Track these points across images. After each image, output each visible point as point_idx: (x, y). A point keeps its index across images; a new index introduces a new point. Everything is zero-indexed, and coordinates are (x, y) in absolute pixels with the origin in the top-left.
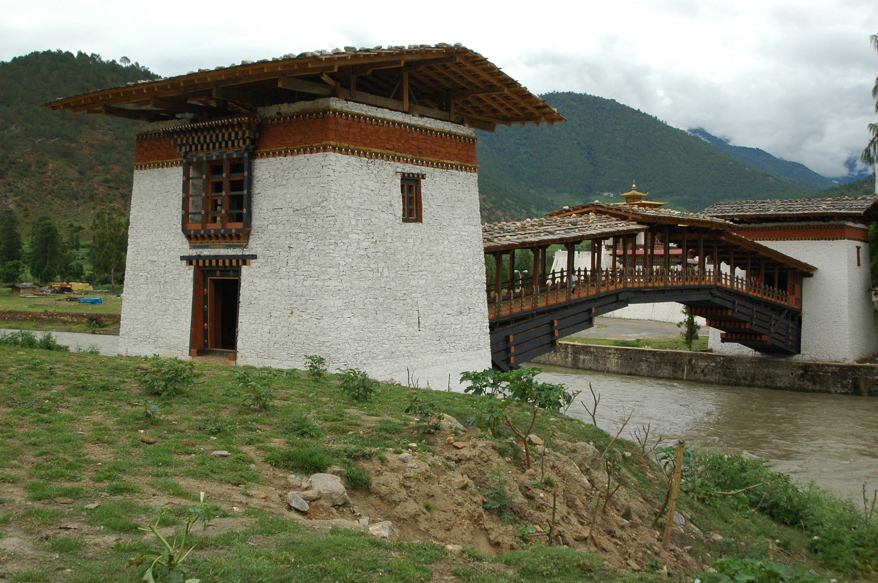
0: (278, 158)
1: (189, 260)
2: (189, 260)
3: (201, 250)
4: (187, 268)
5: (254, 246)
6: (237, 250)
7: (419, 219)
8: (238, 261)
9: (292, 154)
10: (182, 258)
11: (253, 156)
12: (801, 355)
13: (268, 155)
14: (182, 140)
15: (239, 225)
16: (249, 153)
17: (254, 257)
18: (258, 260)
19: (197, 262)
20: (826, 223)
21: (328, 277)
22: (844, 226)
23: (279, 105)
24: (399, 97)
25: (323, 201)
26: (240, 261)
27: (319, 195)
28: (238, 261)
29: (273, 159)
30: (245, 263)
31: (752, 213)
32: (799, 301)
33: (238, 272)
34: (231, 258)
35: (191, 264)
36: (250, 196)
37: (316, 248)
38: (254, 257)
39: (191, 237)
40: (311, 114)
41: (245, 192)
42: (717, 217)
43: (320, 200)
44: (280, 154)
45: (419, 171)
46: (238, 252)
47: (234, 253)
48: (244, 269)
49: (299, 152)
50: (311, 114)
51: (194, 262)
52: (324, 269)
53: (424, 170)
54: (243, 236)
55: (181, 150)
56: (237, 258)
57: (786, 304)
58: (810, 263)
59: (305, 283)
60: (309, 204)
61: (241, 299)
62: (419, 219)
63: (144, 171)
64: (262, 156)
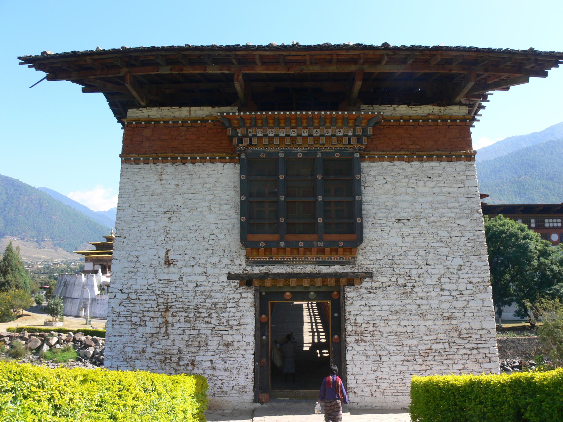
0: (397, 163)
8: (337, 281)
10: (231, 277)
17: (369, 275)
26: (343, 281)
38: (369, 275)
44: (401, 159)
46: (347, 269)
48: (350, 293)
49: (430, 159)
51: (256, 283)
56: (337, 276)
64: (372, 159)
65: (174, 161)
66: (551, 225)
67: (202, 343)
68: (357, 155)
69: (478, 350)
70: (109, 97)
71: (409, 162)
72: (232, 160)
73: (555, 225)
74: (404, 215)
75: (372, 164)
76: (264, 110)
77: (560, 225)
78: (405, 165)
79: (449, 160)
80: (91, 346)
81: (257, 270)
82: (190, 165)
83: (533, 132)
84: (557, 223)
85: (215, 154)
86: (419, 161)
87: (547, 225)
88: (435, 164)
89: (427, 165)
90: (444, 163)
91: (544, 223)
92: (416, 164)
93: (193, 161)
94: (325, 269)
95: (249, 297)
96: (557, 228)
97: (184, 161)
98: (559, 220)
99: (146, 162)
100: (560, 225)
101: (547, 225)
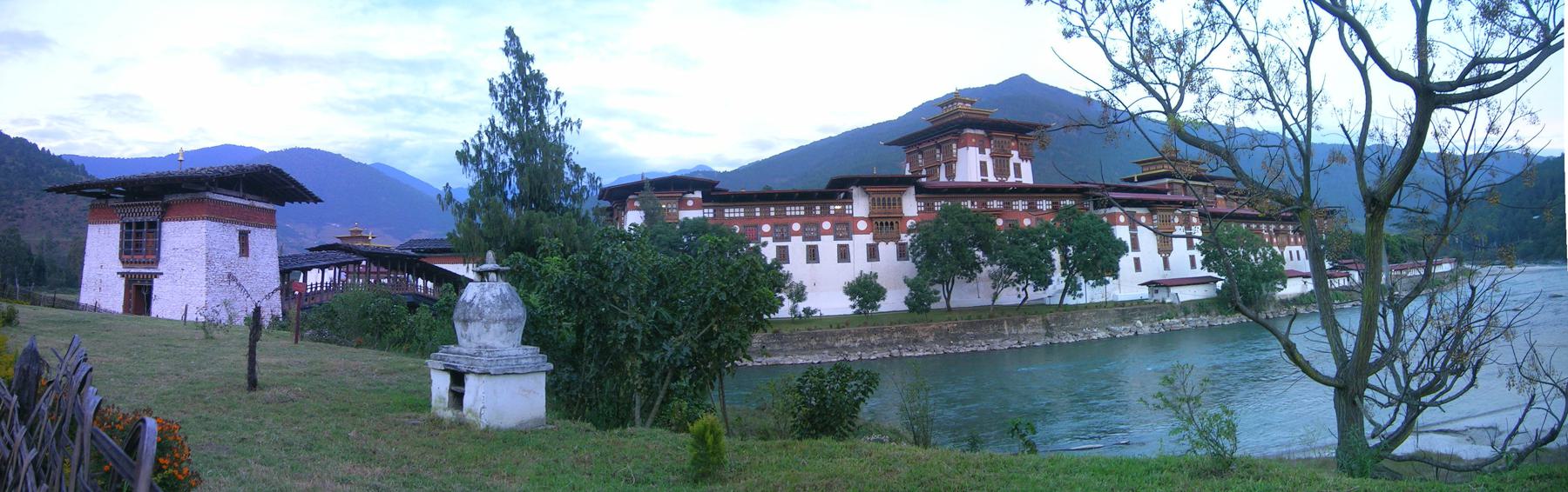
1: (122, 275)
2: (122, 275)
5: (161, 268)
7: (247, 256)
10: (118, 273)
11: (162, 220)
17: (162, 274)
24: (238, 190)
33: (151, 281)
38: (162, 274)
48: (155, 280)
53: (250, 228)
54: (156, 262)
56: (151, 274)
66: (793, 213)
69: (1257, 317)
73: (798, 213)
74: (176, 247)
77: (802, 213)
79: (195, 220)
80: (1330, 269)
81: (126, 270)
83: (988, 84)
84: (739, 212)
87: (727, 215)
91: (724, 213)
92: (183, 222)
94: (132, 271)
95: (123, 281)
96: (800, 216)
98: (802, 208)
100: (802, 213)
101: (788, 213)
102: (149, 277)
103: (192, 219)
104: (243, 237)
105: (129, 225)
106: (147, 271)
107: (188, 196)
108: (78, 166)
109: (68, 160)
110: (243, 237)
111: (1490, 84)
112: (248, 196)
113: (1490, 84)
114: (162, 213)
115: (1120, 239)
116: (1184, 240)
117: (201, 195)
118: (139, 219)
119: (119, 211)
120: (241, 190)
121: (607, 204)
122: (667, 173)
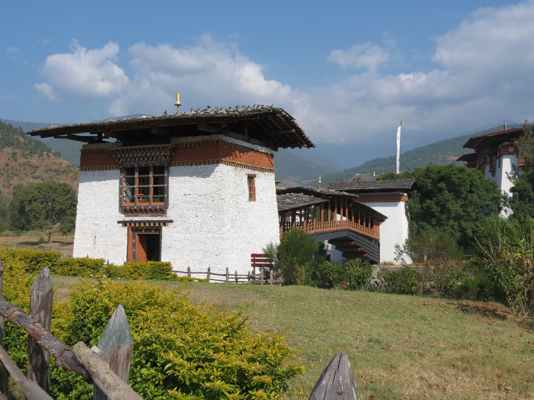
0: (186, 166)
1: (124, 223)
2: (124, 223)
3: (134, 218)
4: (122, 228)
5: (170, 214)
6: (159, 217)
7: (254, 200)
8: (159, 224)
9: (196, 164)
10: (119, 222)
11: (170, 165)
12: (171, 261)
13: (179, 165)
14: (121, 155)
15: (162, 204)
16: (167, 163)
17: (171, 221)
18: (174, 223)
19: (130, 224)
20: (390, 193)
21: (222, 232)
22: (399, 194)
23: (186, 137)
24: (243, 134)
25: (218, 191)
26: (162, 224)
27: (215, 187)
28: (159, 224)
29: (182, 167)
30: (165, 225)
31: (354, 189)
32: (378, 234)
33: (159, 230)
34: (154, 222)
35: (125, 225)
36: (168, 186)
37: (214, 216)
38: (171, 221)
39: (124, 210)
40: (208, 143)
41: (166, 185)
42: (346, 191)
43: (215, 190)
44: (187, 164)
45: (254, 173)
46: (159, 218)
47: (157, 219)
48: (164, 229)
49: (200, 164)
50: (208, 143)
51: (128, 224)
52: (220, 228)
53: (256, 172)
54: (162, 211)
55: (119, 160)
56: (159, 222)
57: (373, 236)
58: (383, 214)
59: (207, 236)
60: (209, 192)
61: (163, 245)
62: (254, 200)
63: (101, 171)
64: (175, 165)
65: (99, 169)
67: (453, 397)
68: (166, 164)
70: (510, 160)
71: (191, 166)
72: (116, 168)
75: (175, 168)
76: (133, 146)
78: (189, 167)
81: (128, 219)
82: (104, 171)
85: (114, 165)
86: (196, 165)
88: (202, 166)
89: (199, 167)
90: (206, 165)
92: (194, 167)
93: (106, 169)
95: (125, 230)
97: (102, 169)
99: (89, 170)
102: (157, 225)
103: (205, 163)
104: (251, 178)
105: (130, 171)
106: (154, 219)
107: (199, 139)
108: (16, 129)
109: (7, 124)
110: (251, 178)
111: (88, 134)
112: (253, 140)
113: (88, 134)
114: (170, 157)
115: (168, 264)
116: (211, 272)
117: (214, 137)
118: (143, 164)
119: (119, 156)
120: (247, 135)
121: (472, 151)
122: (516, 125)
